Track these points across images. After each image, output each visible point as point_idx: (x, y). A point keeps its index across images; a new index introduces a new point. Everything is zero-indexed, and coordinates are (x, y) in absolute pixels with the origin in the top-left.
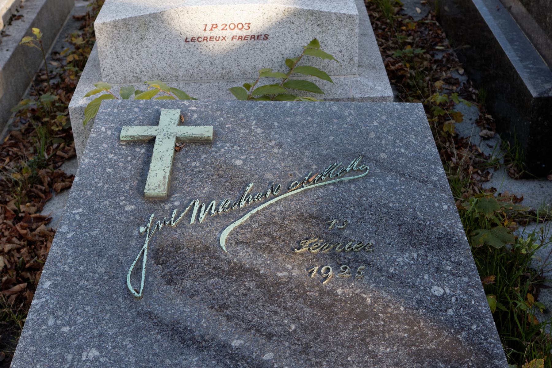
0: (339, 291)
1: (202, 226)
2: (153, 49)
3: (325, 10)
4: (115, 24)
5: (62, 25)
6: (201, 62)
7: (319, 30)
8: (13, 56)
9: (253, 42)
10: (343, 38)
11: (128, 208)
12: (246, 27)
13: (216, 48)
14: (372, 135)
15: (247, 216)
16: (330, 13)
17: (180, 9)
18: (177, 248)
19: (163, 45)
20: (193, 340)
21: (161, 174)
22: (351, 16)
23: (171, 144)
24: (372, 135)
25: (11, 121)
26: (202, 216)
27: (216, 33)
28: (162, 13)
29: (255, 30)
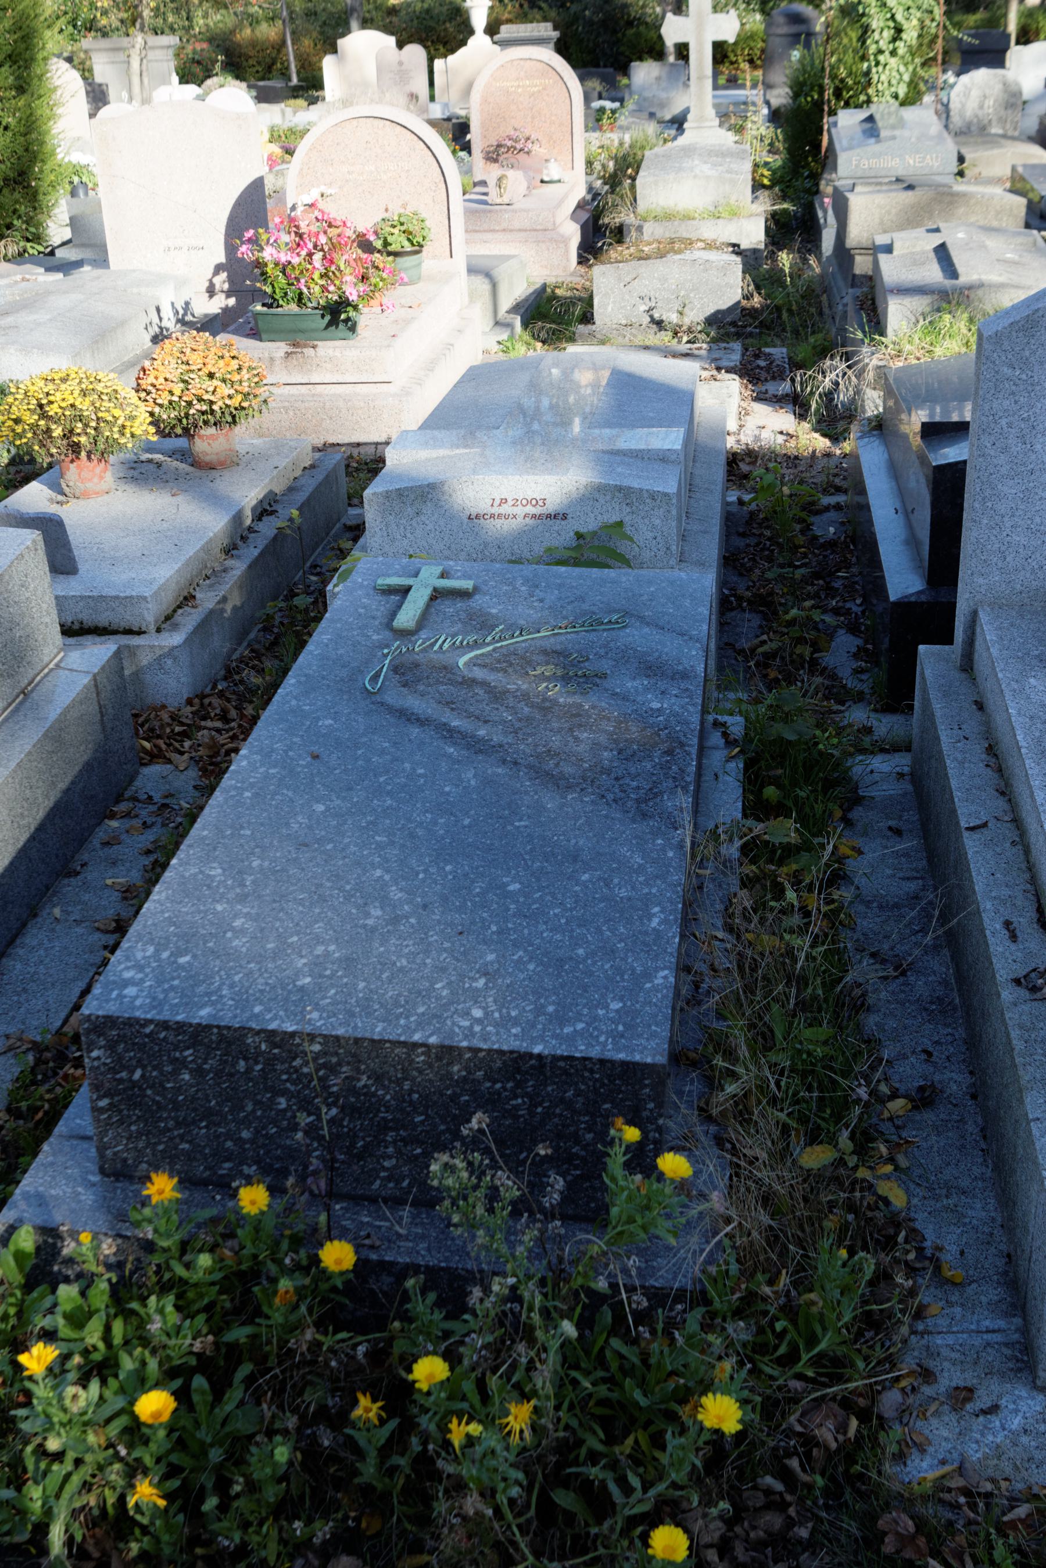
0: (561, 700)
1: (444, 653)
2: (430, 527)
3: (636, 486)
4: (387, 495)
5: (327, 534)
6: (486, 545)
7: (628, 510)
8: (262, 554)
9: (549, 522)
10: (658, 522)
11: (375, 637)
12: (541, 503)
13: (505, 528)
14: (645, 597)
15: (490, 648)
16: (641, 490)
17: (464, 479)
18: (417, 665)
19: (442, 523)
20: (418, 720)
21: (411, 613)
22: (666, 495)
23: (427, 593)
24: (645, 597)
25: (252, 635)
26: (446, 646)
27: (506, 509)
28: (442, 483)
29: (551, 508)
